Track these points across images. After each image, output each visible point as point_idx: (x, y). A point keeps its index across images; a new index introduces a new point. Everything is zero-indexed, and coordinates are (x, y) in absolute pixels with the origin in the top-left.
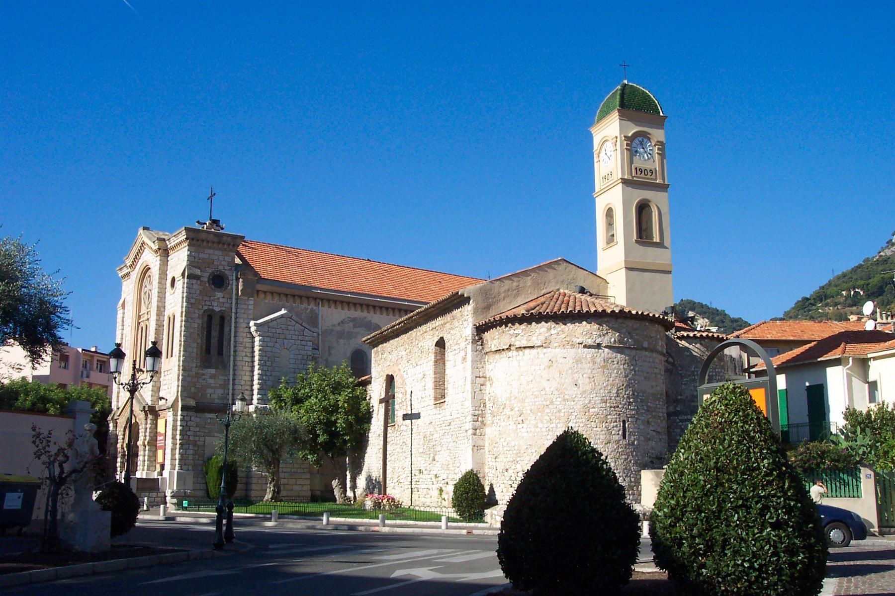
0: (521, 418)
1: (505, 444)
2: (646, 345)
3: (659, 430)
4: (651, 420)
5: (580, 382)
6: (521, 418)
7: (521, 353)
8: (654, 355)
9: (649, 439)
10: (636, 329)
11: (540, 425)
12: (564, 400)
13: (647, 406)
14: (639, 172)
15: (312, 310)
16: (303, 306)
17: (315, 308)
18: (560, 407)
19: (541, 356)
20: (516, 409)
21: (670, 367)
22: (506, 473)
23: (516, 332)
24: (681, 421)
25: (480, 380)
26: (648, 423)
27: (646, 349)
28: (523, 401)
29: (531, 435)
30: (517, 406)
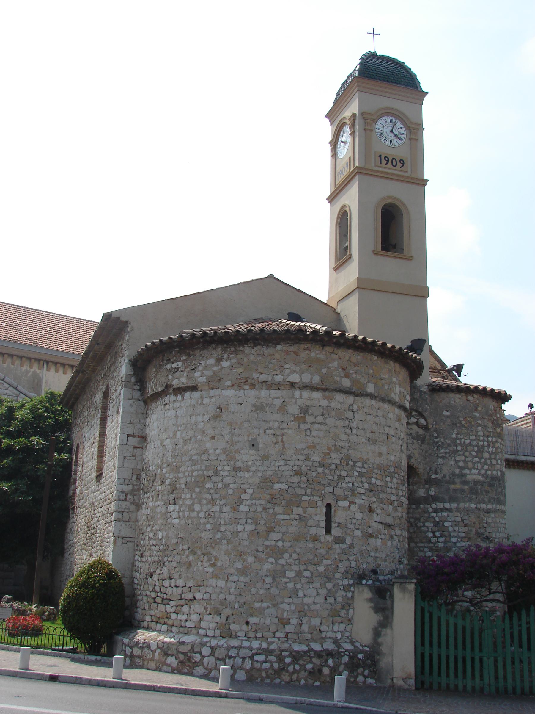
0: (172, 496)
1: (151, 535)
2: (371, 388)
3: (389, 520)
4: (374, 506)
5: (261, 441)
6: (172, 496)
7: (180, 397)
8: (386, 406)
9: (371, 536)
10: (355, 365)
11: (197, 507)
12: (235, 469)
13: (370, 484)
14: (384, 162)
15: (34, 372)
16: (25, 368)
17: (38, 371)
18: (228, 480)
19: (206, 401)
20: (168, 482)
21: (421, 432)
22: (150, 580)
23: (174, 365)
24: (436, 511)
25: (138, 439)
26: (371, 510)
27: (372, 397)
28: (177, 470)
29: (183, 522)
30: (169, 477)
